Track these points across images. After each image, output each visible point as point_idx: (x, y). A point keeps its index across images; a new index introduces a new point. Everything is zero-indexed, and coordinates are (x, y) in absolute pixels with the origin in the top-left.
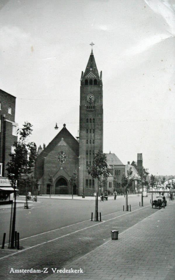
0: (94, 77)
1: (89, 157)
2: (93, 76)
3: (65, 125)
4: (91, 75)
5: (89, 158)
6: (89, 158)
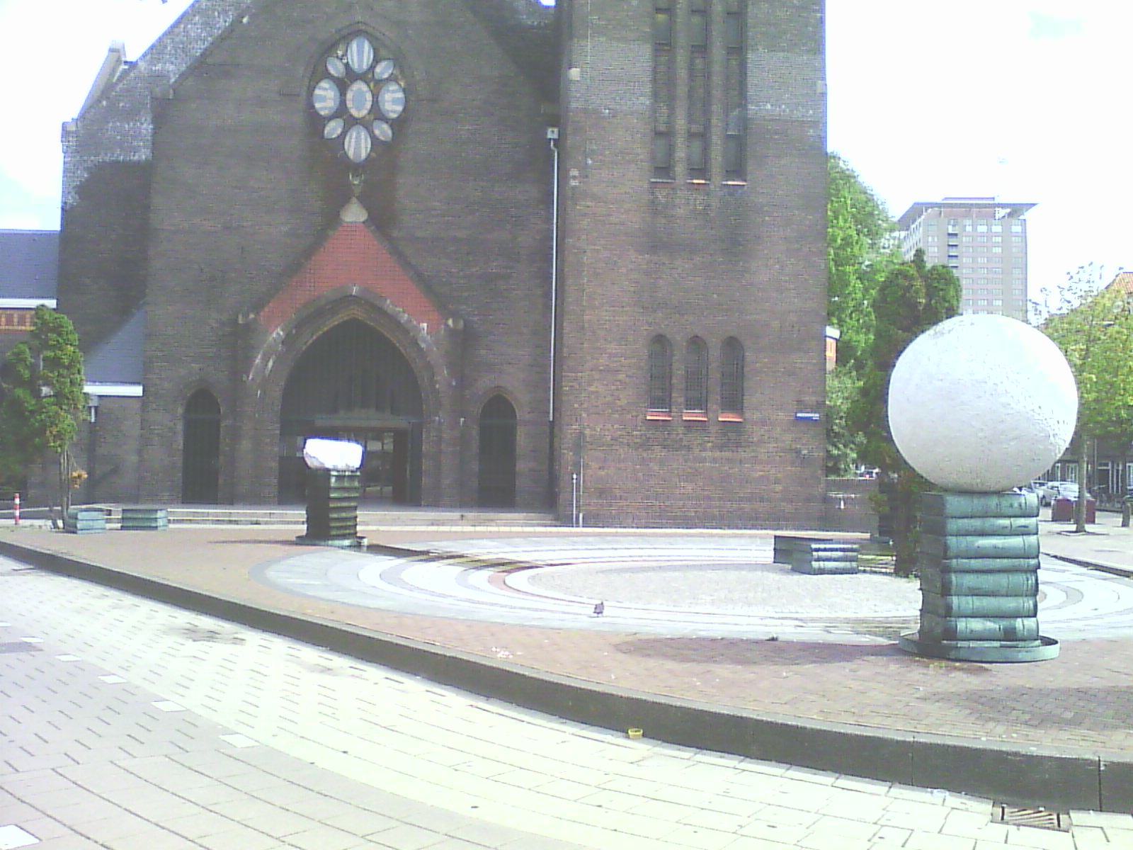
1: (682, 73)
5: (682, 90)
6: (682, 90)
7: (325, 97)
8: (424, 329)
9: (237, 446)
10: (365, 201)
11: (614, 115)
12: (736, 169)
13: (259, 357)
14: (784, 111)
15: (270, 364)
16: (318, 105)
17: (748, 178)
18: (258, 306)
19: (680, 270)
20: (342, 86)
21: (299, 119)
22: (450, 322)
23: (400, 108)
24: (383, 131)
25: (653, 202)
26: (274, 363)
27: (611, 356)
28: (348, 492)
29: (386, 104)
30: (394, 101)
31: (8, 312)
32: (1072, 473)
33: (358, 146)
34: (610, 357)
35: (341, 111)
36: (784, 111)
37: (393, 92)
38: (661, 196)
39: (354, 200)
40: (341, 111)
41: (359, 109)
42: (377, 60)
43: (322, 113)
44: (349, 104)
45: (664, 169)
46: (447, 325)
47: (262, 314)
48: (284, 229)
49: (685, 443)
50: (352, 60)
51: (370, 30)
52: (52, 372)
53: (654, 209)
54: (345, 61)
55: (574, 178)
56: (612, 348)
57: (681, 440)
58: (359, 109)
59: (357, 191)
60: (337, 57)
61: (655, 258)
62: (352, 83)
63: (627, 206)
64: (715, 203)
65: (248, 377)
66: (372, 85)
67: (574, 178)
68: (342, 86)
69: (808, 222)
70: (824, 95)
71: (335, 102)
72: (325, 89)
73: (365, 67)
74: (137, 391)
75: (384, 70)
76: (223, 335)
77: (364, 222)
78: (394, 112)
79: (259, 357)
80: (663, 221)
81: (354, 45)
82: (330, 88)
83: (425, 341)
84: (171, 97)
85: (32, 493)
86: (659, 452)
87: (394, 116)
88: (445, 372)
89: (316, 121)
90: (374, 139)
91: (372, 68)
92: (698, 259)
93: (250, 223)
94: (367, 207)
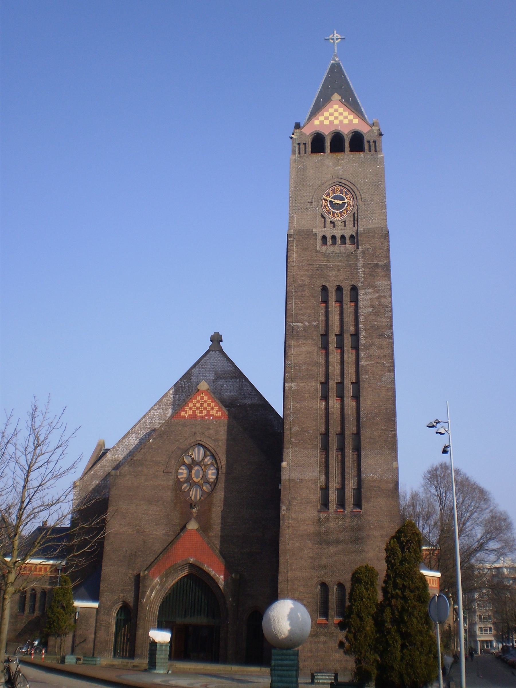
0: (350, 121)
2: (346, 118)
3: (216, 339)
4: (336, 114)
7: (183, 473)
8: (221, 579)
9: (31, 604)
10: (198, 519)
11: (302, 481)
12: (358, 503)
13: (149, 591)
14: (378, 477)
15: (153, 594)
16: (179, 477)
17: (363, 508)
18: (148, 568)
19: (332, 552)
20: (190, 468)
21: (171, 483)
22: (233, 575)
23: (214, 477)
24: (206, 488)
25: (319, 521)
26: (156, 594)
27: (300, 592)
28: (31, 607)
29: (209, 475)
30: (213, 474)
31: (45, 566)
32: (155, 610)
33: (195, 494)
34: (299, 594)
35: (189, 479)
36: (378, 477)
37: (212, 470)
38: (323, 517)
39: (193, 519)
40: (189, 479)
41: (197, 478)
42: (205, 456)
43: (181, 480)
44: (193, 476)
45: (325, 504)
46: (232, 577)
47: (151, 571)
48: (163, 532)
49: (335, 634)
50: (195, 456)
51: (203, 443)
52: (498, 641)
53: (320, 523)
54: (192, 457)
55: (284, 510)
56: (301, 589)
57: (333, 633)
58: (197, 478)
59: (195, 515)
60: (188, 455)
61: (320, 546)
62: (194, 466)
63: (307, 523)
64: (348, 520)
65: (143, 601)
66: (203, 467)
67: (284, 510)
68: (190, 468)
69: (391, 528)
70: (397, 468)
71: (187, 474)
72: (183, 470)
73: (201, 459)
74: (439, 575)
75: (208, 460)
76: (463, 565)
77: (196, 530)
78: (212, 478)
79: (149, 589)
80: (324, 529)
81: (196, 450)
82: (185, 469)
83: (508, 579)
84: (118, 475)
85: (49, 649)
86: (323, 639)
87: (212, 480)
88: (230, 599)
89: (178, 483)
90: (203, 491)
91: (203, 460)
92: (340, 547)
93: (148, 530)
94: (199, 522)
